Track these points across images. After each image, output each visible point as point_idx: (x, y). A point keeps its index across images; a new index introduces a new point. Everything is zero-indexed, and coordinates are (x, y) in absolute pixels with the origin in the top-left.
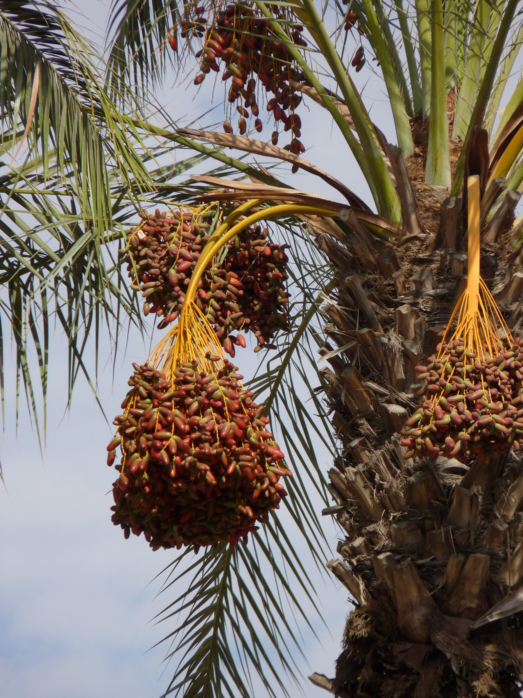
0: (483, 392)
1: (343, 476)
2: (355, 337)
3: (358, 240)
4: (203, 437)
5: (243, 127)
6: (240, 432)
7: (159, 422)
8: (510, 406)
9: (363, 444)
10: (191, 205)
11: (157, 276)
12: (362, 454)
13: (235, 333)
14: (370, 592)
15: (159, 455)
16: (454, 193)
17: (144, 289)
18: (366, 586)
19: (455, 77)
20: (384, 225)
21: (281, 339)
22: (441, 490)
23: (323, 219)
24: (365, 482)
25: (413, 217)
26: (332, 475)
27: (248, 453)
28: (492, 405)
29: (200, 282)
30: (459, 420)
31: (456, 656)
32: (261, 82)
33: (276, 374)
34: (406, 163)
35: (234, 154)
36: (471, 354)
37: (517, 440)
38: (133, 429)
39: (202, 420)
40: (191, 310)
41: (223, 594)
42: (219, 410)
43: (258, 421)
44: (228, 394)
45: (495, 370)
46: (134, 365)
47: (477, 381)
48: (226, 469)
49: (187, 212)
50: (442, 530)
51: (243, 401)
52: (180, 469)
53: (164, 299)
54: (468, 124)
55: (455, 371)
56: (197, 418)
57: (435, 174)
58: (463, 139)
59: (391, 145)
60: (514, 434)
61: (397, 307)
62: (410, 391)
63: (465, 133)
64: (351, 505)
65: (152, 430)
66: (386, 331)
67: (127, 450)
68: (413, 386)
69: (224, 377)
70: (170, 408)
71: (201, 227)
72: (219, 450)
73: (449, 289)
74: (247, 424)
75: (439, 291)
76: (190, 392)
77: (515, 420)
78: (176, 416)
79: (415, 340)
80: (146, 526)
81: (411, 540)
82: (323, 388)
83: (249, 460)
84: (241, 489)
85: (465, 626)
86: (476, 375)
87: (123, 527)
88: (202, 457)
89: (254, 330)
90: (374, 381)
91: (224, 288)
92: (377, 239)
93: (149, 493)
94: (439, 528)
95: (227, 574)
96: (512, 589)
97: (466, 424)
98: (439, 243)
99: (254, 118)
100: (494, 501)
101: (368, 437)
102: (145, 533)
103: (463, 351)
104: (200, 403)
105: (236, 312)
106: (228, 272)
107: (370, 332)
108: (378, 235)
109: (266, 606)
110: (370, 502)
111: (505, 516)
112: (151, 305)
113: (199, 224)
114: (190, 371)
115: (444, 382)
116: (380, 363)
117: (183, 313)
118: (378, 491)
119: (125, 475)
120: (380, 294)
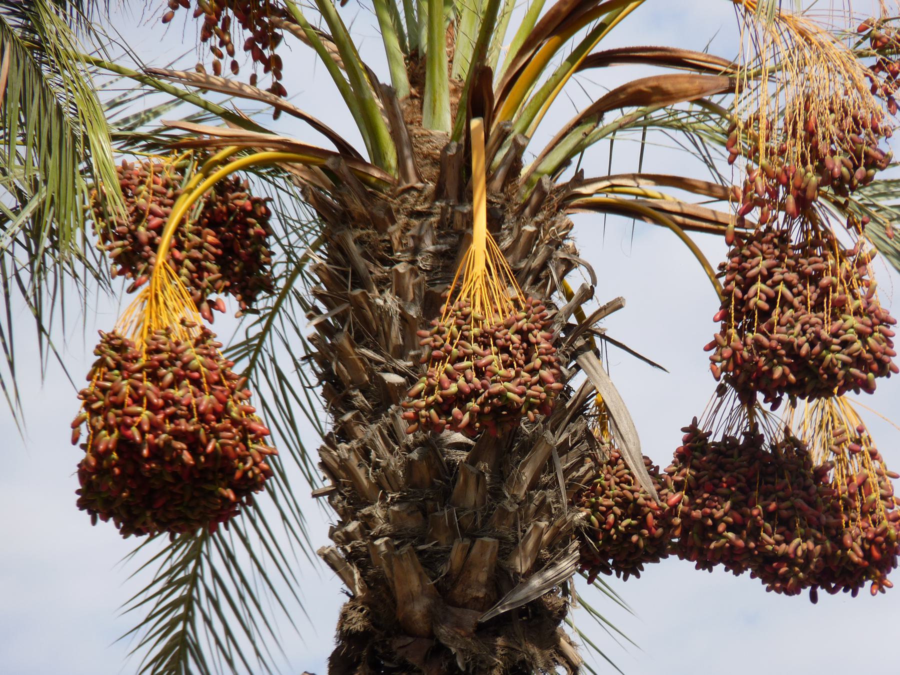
0: (493, 358)
1: (335, 454)
2: (347, 298)
3: (349, 192)
4: (179, 412)
5: (217, 69)
6: (220, 407)
7: (130, 396)
8: (523, 373)
9: (357, 417)
10: (162, 155)
11: (125, 234)
12: (356, 429)
13: (213, 297)
14: (366, 582)
15: (129, 432)
16: (456, 136)
17: (111, 249)
18: (361, 575)
19: (455, 9)
20: (376, 174)
21: (263, 301)
22: (443, 467)
23: (309, 168)
24: (359, 460)
25: (410, 164)
26: (322, 453)
27: (228, 430)
28: (503, 372)
29: (173, 241)
30: (468, 390)
31: (462, 651)
32: (236, 19)
33: (256, 342)
34: (402, 105)
35: (213, 98)
36: (479, 316)
37: (532, 411)
38: (100, 403)
39: (177, 393)
40: (163, 270)
41: (194, 584)
42: (196, 382)
43: (239, 393)
44: (206, 364)
45: (506, 334)
46: (100, 332)
47: (486, 346)
48: (205, 447)
49: (157, 163)
50: (446, 511)
51: (223, 371)
52: (154, 448)
53: (132, 259)
54: (470, 61)
55: (462, 335)
56: (172, 391)
57: (434, 118)
58: (464, 78)
59: (385, 85)
60: (527, 404)
61: (393, 265)
62: (409, 358)
63: (467, 72)
64: (345, 486)
65: (120, 405)
66: (381, 292)
67: (93, 427)
68: (412, 353)
69: (202, 345)
70: (141, 380)
71: (173, 180)
72: (197, 426)
73: (451, 245)
74: (228, 397)
75: (439, 247)
76: (164, 362)
77: (529, 388)
78: (149, 389)
79: (413, 301)
80: (116, 511)
81: (411, 523)
82: (307, 358)
83: (231, 437)
84: (221, 470)
85: (472, 618)
86: (485, 339)
87: (90, 512)
88: (177, 435)
89: (235, 294)
90: (368, 348)
91: (200, 247)
92: (369, 190)
93: (119, 475)
94: (442, 510)
95: (199, 563)
96: (524, 576)
97: (475, 393)
98: (439, 193)
99: (230, 59)
100: (503, 479)
101: (362, 410)
102: (114, 520)
103: (470, 313)
104: (175, 374)
105: (214, 274)
106: (204, 228)
107: (364, 293)
108: (371, 186)
109: (242, 598)
110: (365, 482)
111: (515, 495)
112: (119, 267)
113: (169, 175)
114: (163, 338)
115: (450, 347)
116: (375, 327)
117: (154, 275)
118: (374, 469)
119: (93, 456)
120: (374, 251)
